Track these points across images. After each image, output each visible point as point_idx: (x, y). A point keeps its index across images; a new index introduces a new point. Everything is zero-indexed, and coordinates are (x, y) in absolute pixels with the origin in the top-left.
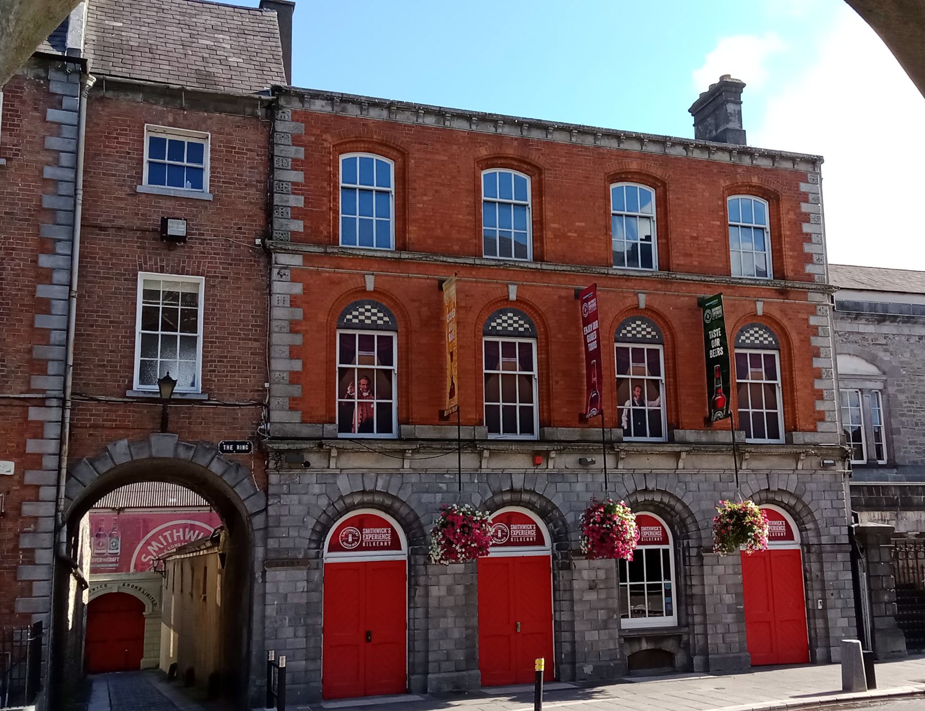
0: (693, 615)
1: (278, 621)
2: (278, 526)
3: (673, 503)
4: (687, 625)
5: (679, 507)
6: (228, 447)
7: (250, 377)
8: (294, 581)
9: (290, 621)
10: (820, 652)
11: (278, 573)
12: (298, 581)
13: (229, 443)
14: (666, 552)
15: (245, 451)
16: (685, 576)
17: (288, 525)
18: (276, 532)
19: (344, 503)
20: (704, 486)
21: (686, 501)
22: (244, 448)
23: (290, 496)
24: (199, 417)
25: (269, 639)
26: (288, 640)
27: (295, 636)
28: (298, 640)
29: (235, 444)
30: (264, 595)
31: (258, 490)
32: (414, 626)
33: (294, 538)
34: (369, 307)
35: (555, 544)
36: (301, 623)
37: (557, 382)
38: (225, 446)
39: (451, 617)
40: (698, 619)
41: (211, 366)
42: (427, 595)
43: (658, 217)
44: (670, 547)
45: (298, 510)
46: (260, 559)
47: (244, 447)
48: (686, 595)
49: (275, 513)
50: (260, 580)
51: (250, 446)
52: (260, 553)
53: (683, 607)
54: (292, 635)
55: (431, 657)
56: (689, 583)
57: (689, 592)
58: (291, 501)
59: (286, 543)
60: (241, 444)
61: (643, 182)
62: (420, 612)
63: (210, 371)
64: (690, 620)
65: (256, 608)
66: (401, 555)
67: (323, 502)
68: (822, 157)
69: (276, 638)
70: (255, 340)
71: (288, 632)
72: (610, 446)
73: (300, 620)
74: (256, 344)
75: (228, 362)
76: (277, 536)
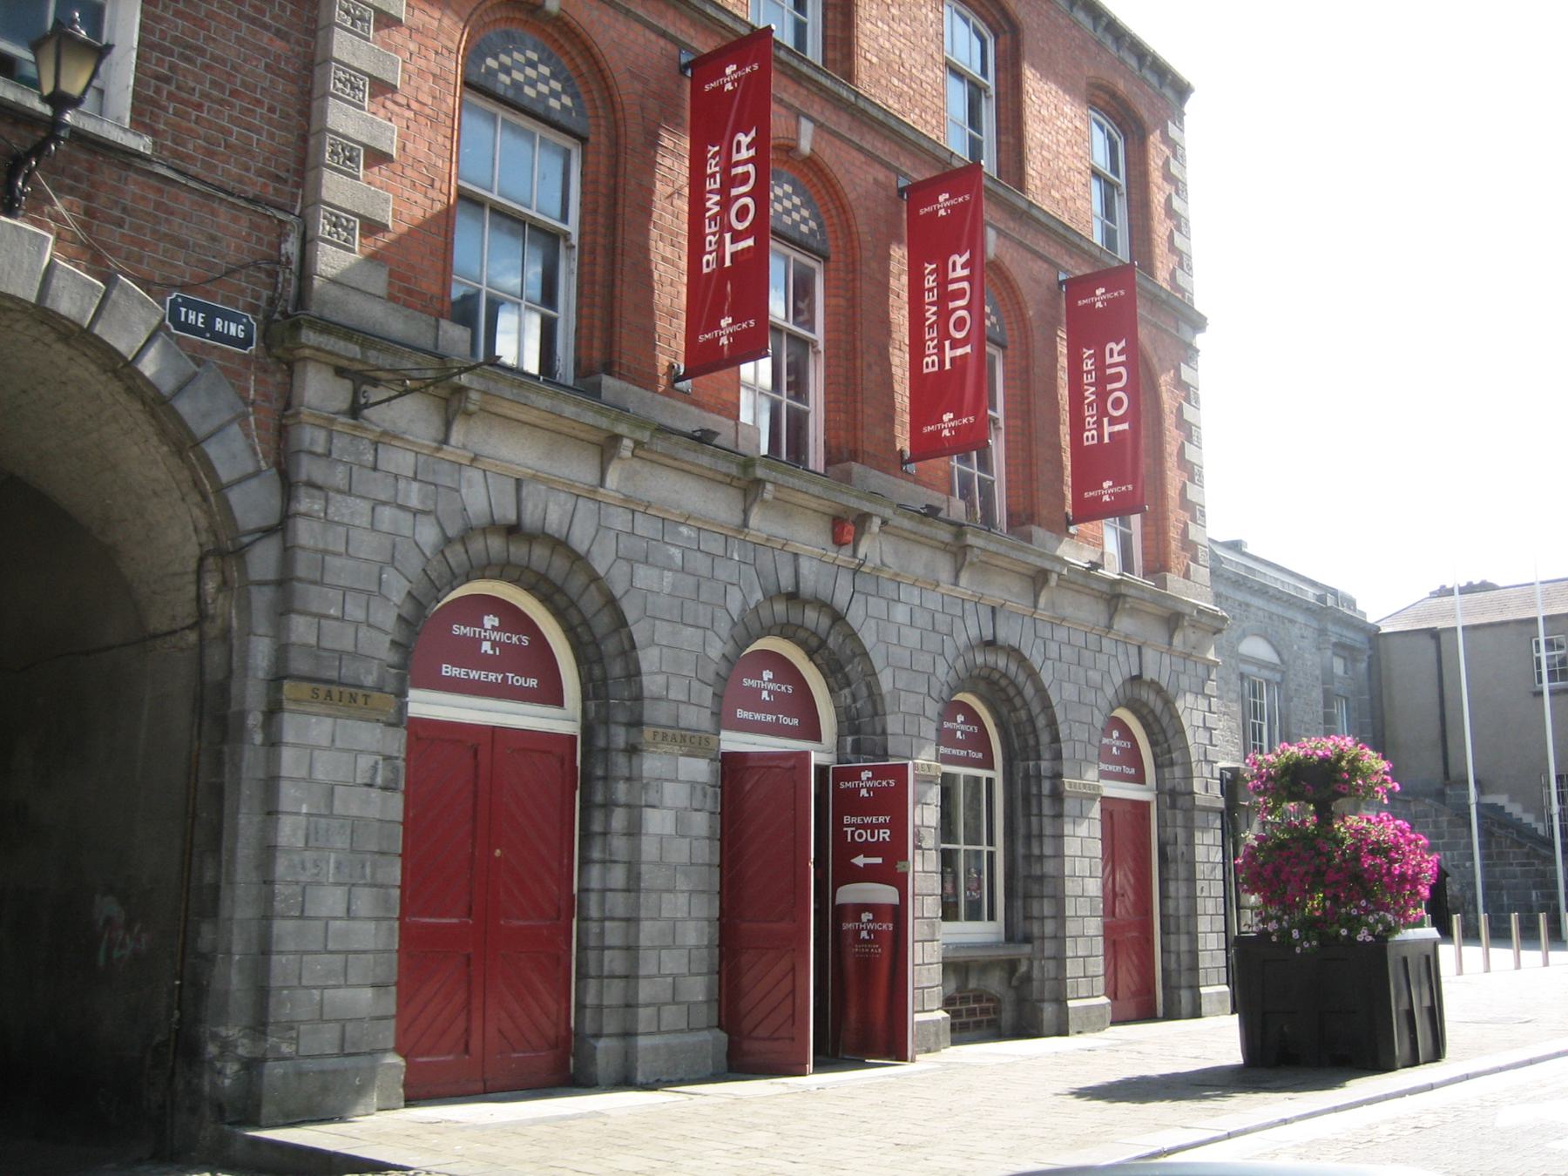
0: (1042, 919)
1: (309, 865)
2: (319, 583)
3: (1021, 678)
4: (1028, 939)
5: (1029, 691)
6: (192, 317)
7: (258, 131)
8: (349, 750)
9: (339, 865)
10: (606, 1051)
11: (314, 720)
12: (361, 752)
13: (198, 307)
14: (990, 781)
15: (233, 341)
16: (1028, 837)
17: (342, 583)
18: (313, 597)
19: (467, 552)
20: (1066, 651)
21: (1046, 677)
22: (233, 332)
23: (350, 500)
24: (116, 202)
25: (283, 917)
26: (332, 923)
27: (349, 915)
28: (356, 925)
29: (211, 314)
30: (271, 783)
31: (263, 464)
32: (603, 909)
33: (357, 624)
34: (535, 57)
35: (849, 739)
36: (363, 876)
37: (870, 366)
38: (183, 310)
39: (683, 892)
40: (1049, 927)
41: (160, 62)
42: (634, 831)
43: (1002, 90)
44: (997, 775)
45: (367, 545)
46: (261, 675)
47: (233, 327)
48: (1028, 877)
49: (312, 542)
50: (258, 738)
51: (248, 331)
52: (260, 657)
53: (1019, 903)
54: (340, 910)
55: (645, 991)
56: (1036, 851)
57: (1036, 870)
58: (352, 514)
59: (340, 638)
60: (229, 317)
61: (983, 11)
62: (618, 876)
63: (158, 77)
64: (1036, 929)
65: (247, 823)
66: (561, 721)
67: (428, 535)
68: (1182, 90)
69: (302, 917)
70: (279, 33)
71: (330, 901)
72: (557, 597)
73: (363, 867)
74: (279, 46)
75: (207, 67)
76: (314, 609)
